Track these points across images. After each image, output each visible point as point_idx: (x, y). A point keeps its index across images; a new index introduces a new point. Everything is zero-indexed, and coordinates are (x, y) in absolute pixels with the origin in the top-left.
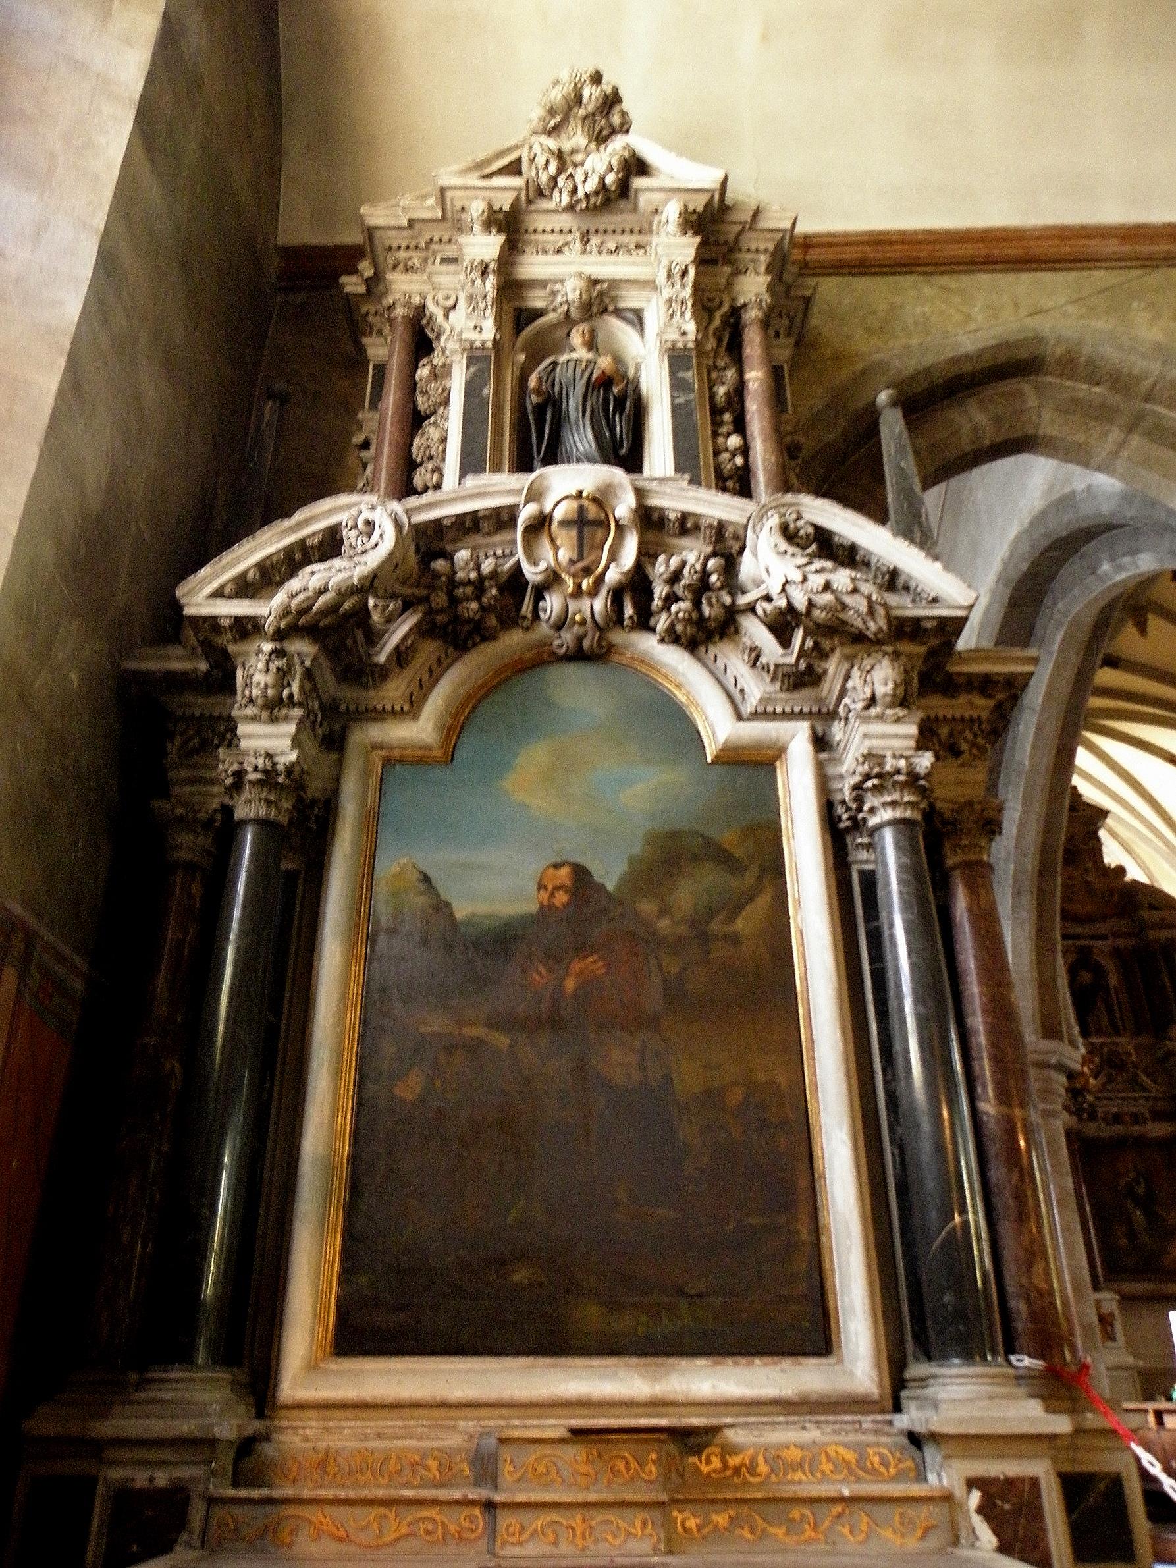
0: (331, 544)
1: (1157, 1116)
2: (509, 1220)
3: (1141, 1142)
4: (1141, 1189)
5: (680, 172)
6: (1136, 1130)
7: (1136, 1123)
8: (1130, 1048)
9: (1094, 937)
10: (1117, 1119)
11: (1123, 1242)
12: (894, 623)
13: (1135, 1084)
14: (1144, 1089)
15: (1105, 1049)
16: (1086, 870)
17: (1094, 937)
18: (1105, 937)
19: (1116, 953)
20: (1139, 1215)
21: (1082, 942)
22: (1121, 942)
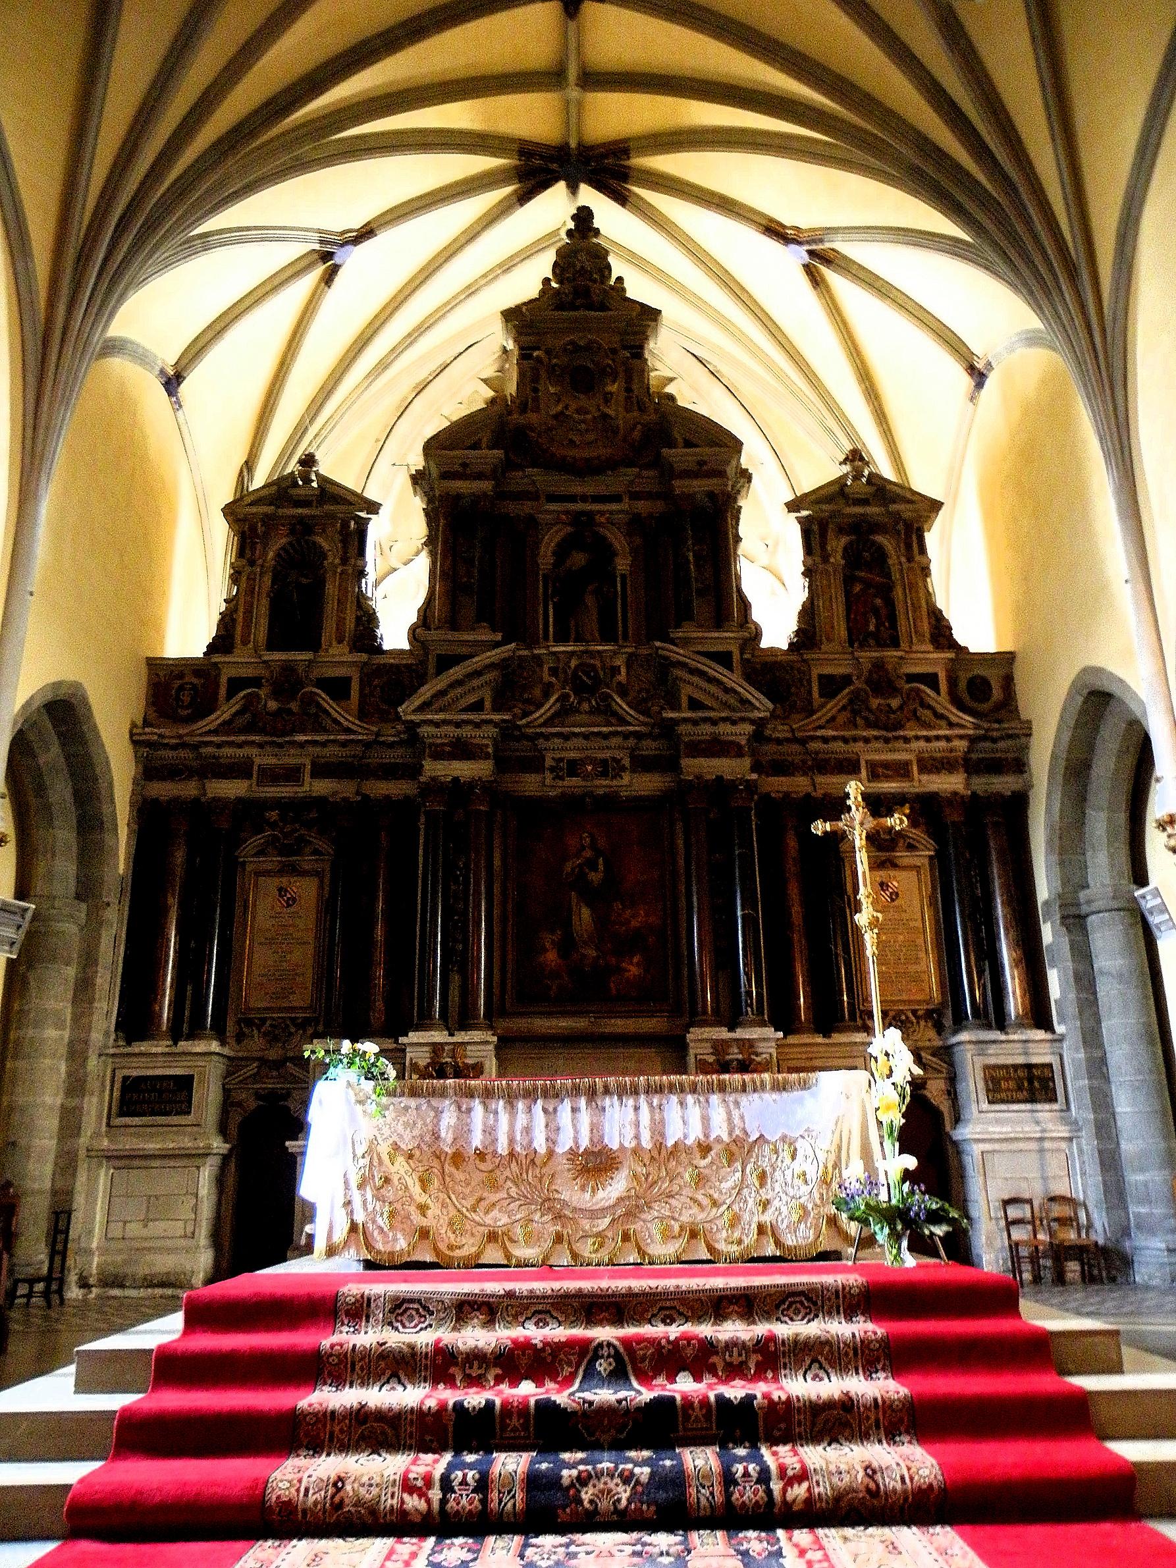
0: (864, 873)
1: (642, 764)
2: (394, 633)
3: (610, 802)
4: (595, 877)
5: (1165, 834)
6: (602, 785)
7: (604, 774)
8: (619, 662)
9: (598, 499)
10: (573, 768)
11: (551, 956)
12: (530, 184)
13: (606, 712)
14: (622, 721)
15: (574, 663)
16: (607, 398)
17: (598, 499)
18: (617, 498)
19: (635, 524)
20: (586, 913)
21: (579, 506)
22: (642, 506)
